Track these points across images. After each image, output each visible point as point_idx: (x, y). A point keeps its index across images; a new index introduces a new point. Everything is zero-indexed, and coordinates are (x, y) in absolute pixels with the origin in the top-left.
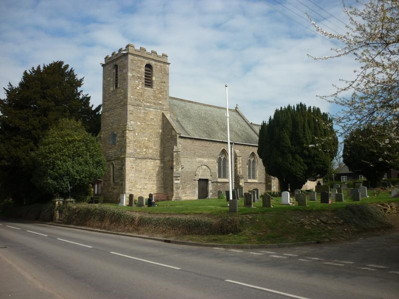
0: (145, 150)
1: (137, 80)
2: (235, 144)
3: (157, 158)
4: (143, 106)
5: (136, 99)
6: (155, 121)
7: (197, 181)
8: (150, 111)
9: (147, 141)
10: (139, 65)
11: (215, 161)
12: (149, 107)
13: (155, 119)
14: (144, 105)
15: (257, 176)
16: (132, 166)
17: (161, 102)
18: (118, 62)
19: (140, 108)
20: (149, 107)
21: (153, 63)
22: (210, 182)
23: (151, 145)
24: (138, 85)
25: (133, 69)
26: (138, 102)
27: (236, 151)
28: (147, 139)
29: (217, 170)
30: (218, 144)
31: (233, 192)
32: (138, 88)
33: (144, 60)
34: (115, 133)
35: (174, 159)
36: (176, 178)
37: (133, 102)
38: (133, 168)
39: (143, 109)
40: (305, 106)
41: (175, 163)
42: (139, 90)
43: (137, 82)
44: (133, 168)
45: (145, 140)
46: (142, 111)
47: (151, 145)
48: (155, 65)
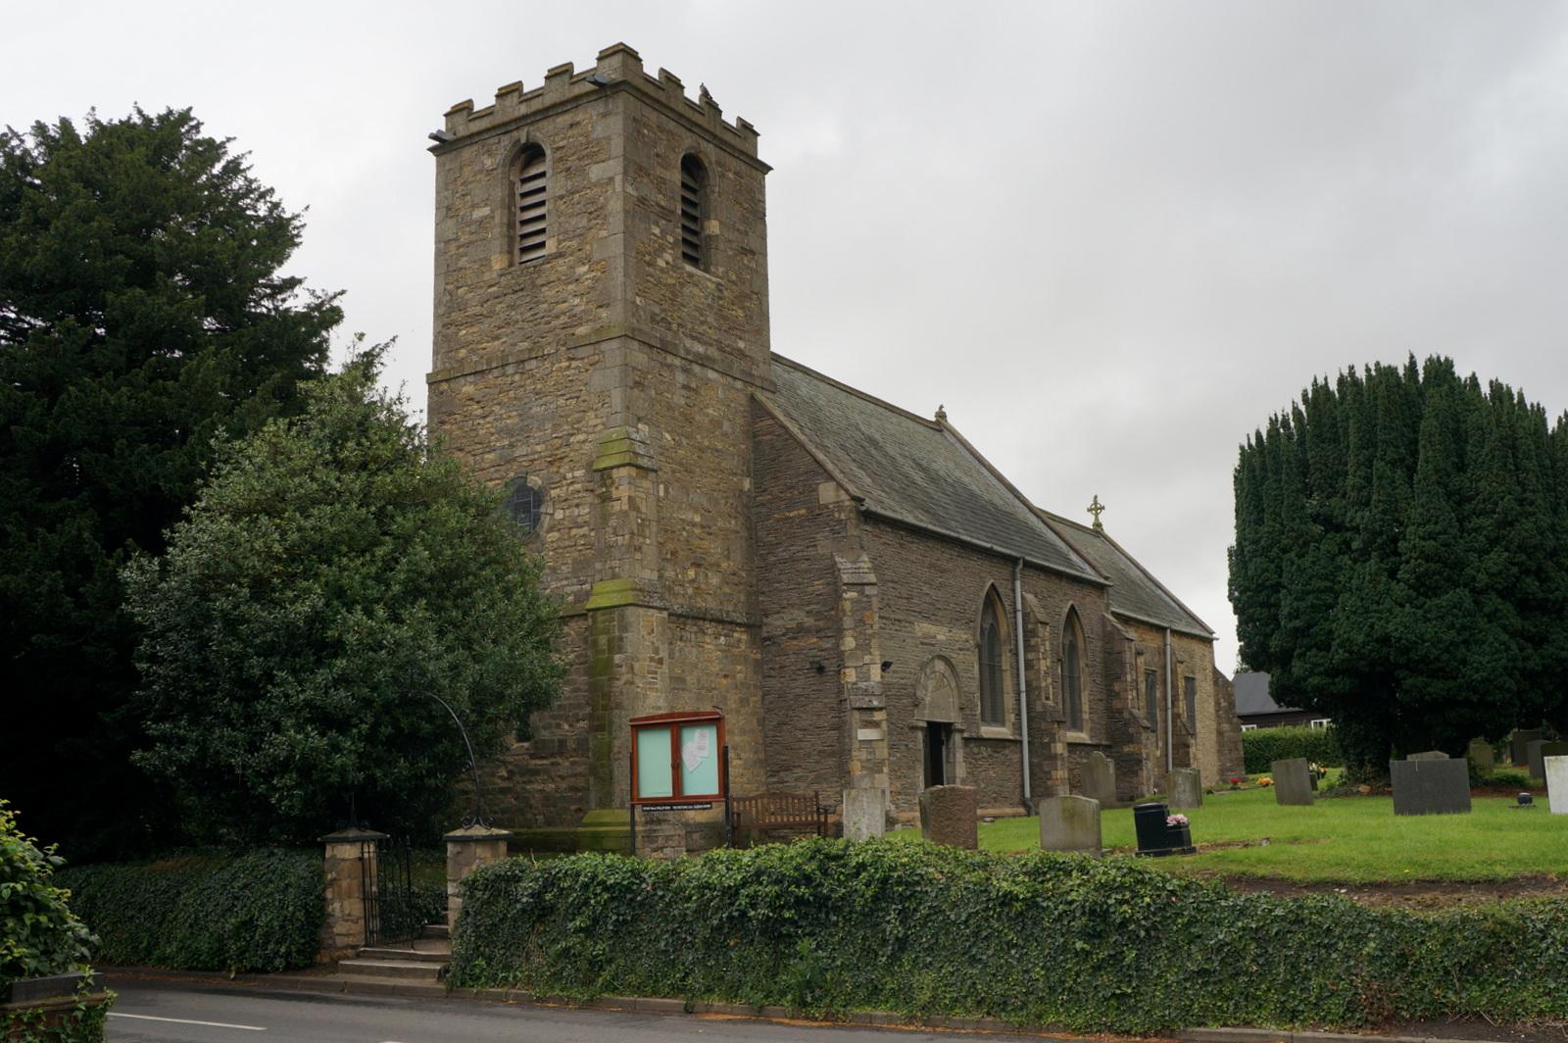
0: (691, 573)
1: (657, 224)
2: (1028, 565)
3: (735, 616)
4: (682, 353)
5: (653, 316)
6: (725, 434)
7: (920, 735)
8: (707, 382)
9: (697, 531)
10: (661, 150)
11: (965, 636)
12: (704, 362)
13: (726, 426)
14: (688, 352)
15: (1086, 716)
16: (656, 651)
17: (741, 345)
18: (543, 134)
19: (670, 359)
20: (704, 362)
21: (710, 153)
22: (957, 738)
23: (714, 548)
24: (662, 249)
25: (641, 169)
26: (660, 331)
27: (1030, 597)
28: (697, 519)
29: (977, 683)
30: (976, 564)
31: (492, 825)
32: (661, 263)
33: (681, 131)
34: (534, 481)
35: (848, 622)
36: (866, 717)
37: (644, 327)
38: (660, 661)
39: (685, 370)
40: (1509, 389)
41: (849, 643)
42: (662, 270)
43: (657, 231)
44: (660, 661)
45: (694, 525)
46: (681, 378)
47: (714, 548)
48: (719, 163)
